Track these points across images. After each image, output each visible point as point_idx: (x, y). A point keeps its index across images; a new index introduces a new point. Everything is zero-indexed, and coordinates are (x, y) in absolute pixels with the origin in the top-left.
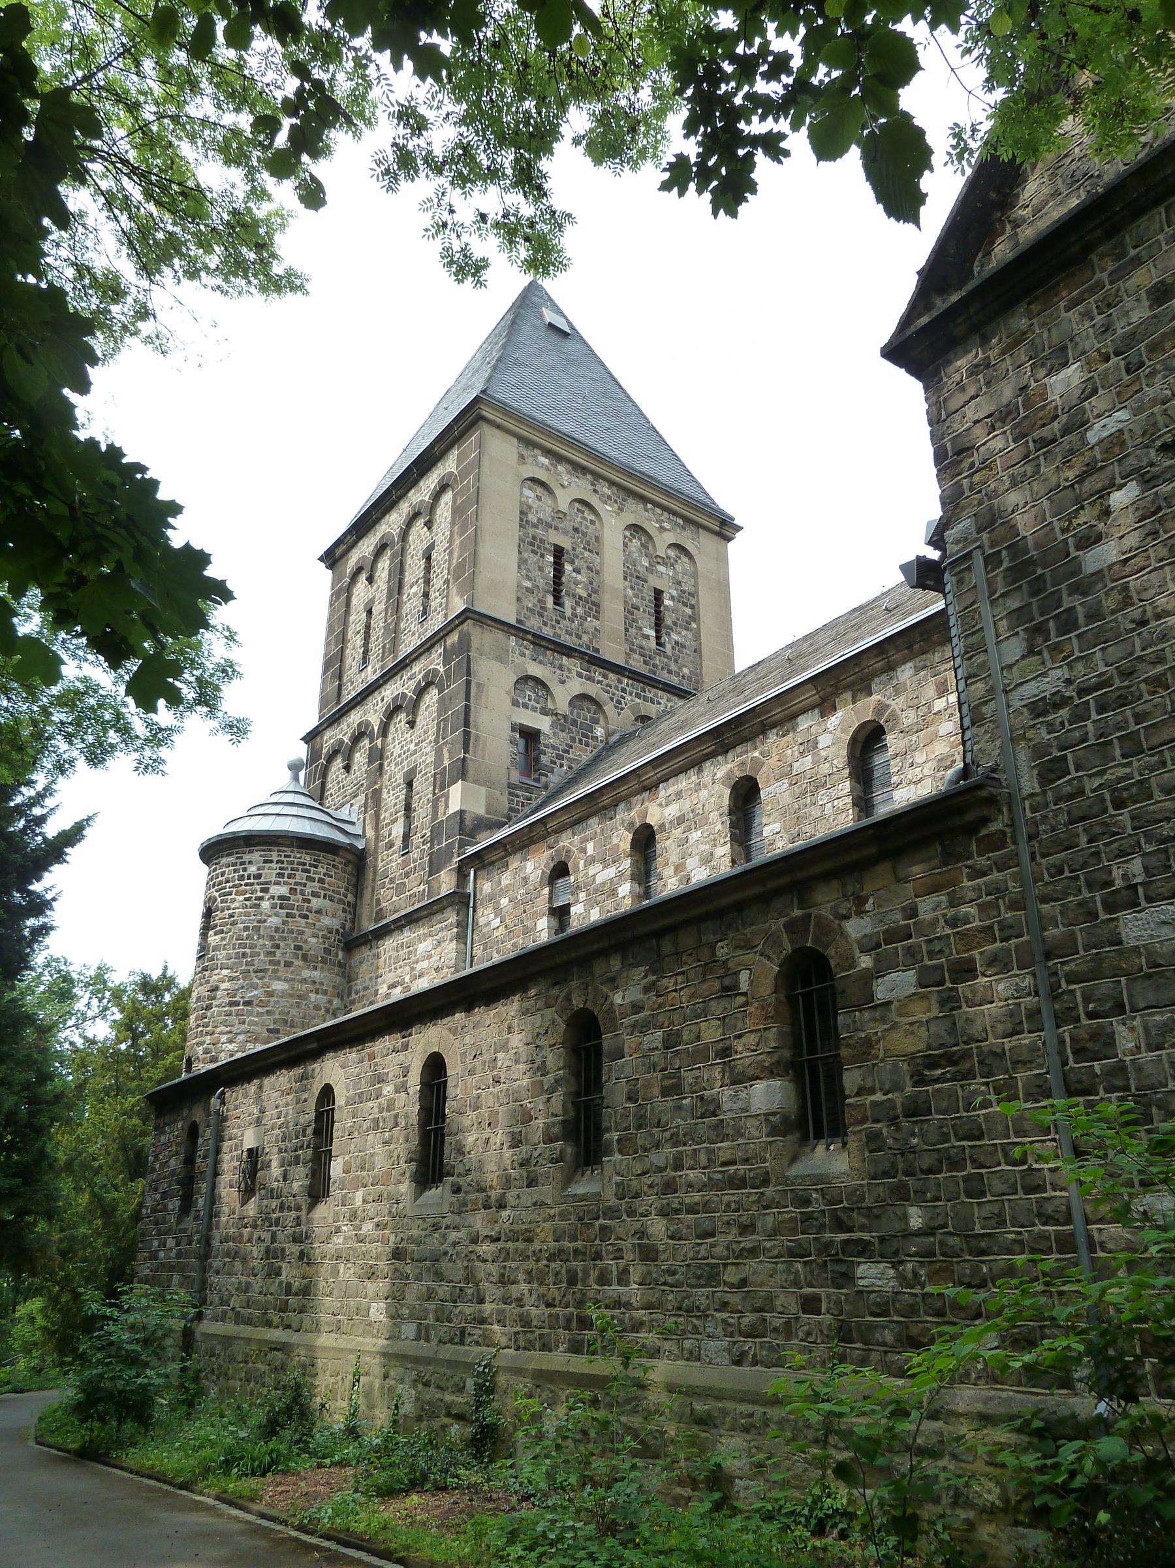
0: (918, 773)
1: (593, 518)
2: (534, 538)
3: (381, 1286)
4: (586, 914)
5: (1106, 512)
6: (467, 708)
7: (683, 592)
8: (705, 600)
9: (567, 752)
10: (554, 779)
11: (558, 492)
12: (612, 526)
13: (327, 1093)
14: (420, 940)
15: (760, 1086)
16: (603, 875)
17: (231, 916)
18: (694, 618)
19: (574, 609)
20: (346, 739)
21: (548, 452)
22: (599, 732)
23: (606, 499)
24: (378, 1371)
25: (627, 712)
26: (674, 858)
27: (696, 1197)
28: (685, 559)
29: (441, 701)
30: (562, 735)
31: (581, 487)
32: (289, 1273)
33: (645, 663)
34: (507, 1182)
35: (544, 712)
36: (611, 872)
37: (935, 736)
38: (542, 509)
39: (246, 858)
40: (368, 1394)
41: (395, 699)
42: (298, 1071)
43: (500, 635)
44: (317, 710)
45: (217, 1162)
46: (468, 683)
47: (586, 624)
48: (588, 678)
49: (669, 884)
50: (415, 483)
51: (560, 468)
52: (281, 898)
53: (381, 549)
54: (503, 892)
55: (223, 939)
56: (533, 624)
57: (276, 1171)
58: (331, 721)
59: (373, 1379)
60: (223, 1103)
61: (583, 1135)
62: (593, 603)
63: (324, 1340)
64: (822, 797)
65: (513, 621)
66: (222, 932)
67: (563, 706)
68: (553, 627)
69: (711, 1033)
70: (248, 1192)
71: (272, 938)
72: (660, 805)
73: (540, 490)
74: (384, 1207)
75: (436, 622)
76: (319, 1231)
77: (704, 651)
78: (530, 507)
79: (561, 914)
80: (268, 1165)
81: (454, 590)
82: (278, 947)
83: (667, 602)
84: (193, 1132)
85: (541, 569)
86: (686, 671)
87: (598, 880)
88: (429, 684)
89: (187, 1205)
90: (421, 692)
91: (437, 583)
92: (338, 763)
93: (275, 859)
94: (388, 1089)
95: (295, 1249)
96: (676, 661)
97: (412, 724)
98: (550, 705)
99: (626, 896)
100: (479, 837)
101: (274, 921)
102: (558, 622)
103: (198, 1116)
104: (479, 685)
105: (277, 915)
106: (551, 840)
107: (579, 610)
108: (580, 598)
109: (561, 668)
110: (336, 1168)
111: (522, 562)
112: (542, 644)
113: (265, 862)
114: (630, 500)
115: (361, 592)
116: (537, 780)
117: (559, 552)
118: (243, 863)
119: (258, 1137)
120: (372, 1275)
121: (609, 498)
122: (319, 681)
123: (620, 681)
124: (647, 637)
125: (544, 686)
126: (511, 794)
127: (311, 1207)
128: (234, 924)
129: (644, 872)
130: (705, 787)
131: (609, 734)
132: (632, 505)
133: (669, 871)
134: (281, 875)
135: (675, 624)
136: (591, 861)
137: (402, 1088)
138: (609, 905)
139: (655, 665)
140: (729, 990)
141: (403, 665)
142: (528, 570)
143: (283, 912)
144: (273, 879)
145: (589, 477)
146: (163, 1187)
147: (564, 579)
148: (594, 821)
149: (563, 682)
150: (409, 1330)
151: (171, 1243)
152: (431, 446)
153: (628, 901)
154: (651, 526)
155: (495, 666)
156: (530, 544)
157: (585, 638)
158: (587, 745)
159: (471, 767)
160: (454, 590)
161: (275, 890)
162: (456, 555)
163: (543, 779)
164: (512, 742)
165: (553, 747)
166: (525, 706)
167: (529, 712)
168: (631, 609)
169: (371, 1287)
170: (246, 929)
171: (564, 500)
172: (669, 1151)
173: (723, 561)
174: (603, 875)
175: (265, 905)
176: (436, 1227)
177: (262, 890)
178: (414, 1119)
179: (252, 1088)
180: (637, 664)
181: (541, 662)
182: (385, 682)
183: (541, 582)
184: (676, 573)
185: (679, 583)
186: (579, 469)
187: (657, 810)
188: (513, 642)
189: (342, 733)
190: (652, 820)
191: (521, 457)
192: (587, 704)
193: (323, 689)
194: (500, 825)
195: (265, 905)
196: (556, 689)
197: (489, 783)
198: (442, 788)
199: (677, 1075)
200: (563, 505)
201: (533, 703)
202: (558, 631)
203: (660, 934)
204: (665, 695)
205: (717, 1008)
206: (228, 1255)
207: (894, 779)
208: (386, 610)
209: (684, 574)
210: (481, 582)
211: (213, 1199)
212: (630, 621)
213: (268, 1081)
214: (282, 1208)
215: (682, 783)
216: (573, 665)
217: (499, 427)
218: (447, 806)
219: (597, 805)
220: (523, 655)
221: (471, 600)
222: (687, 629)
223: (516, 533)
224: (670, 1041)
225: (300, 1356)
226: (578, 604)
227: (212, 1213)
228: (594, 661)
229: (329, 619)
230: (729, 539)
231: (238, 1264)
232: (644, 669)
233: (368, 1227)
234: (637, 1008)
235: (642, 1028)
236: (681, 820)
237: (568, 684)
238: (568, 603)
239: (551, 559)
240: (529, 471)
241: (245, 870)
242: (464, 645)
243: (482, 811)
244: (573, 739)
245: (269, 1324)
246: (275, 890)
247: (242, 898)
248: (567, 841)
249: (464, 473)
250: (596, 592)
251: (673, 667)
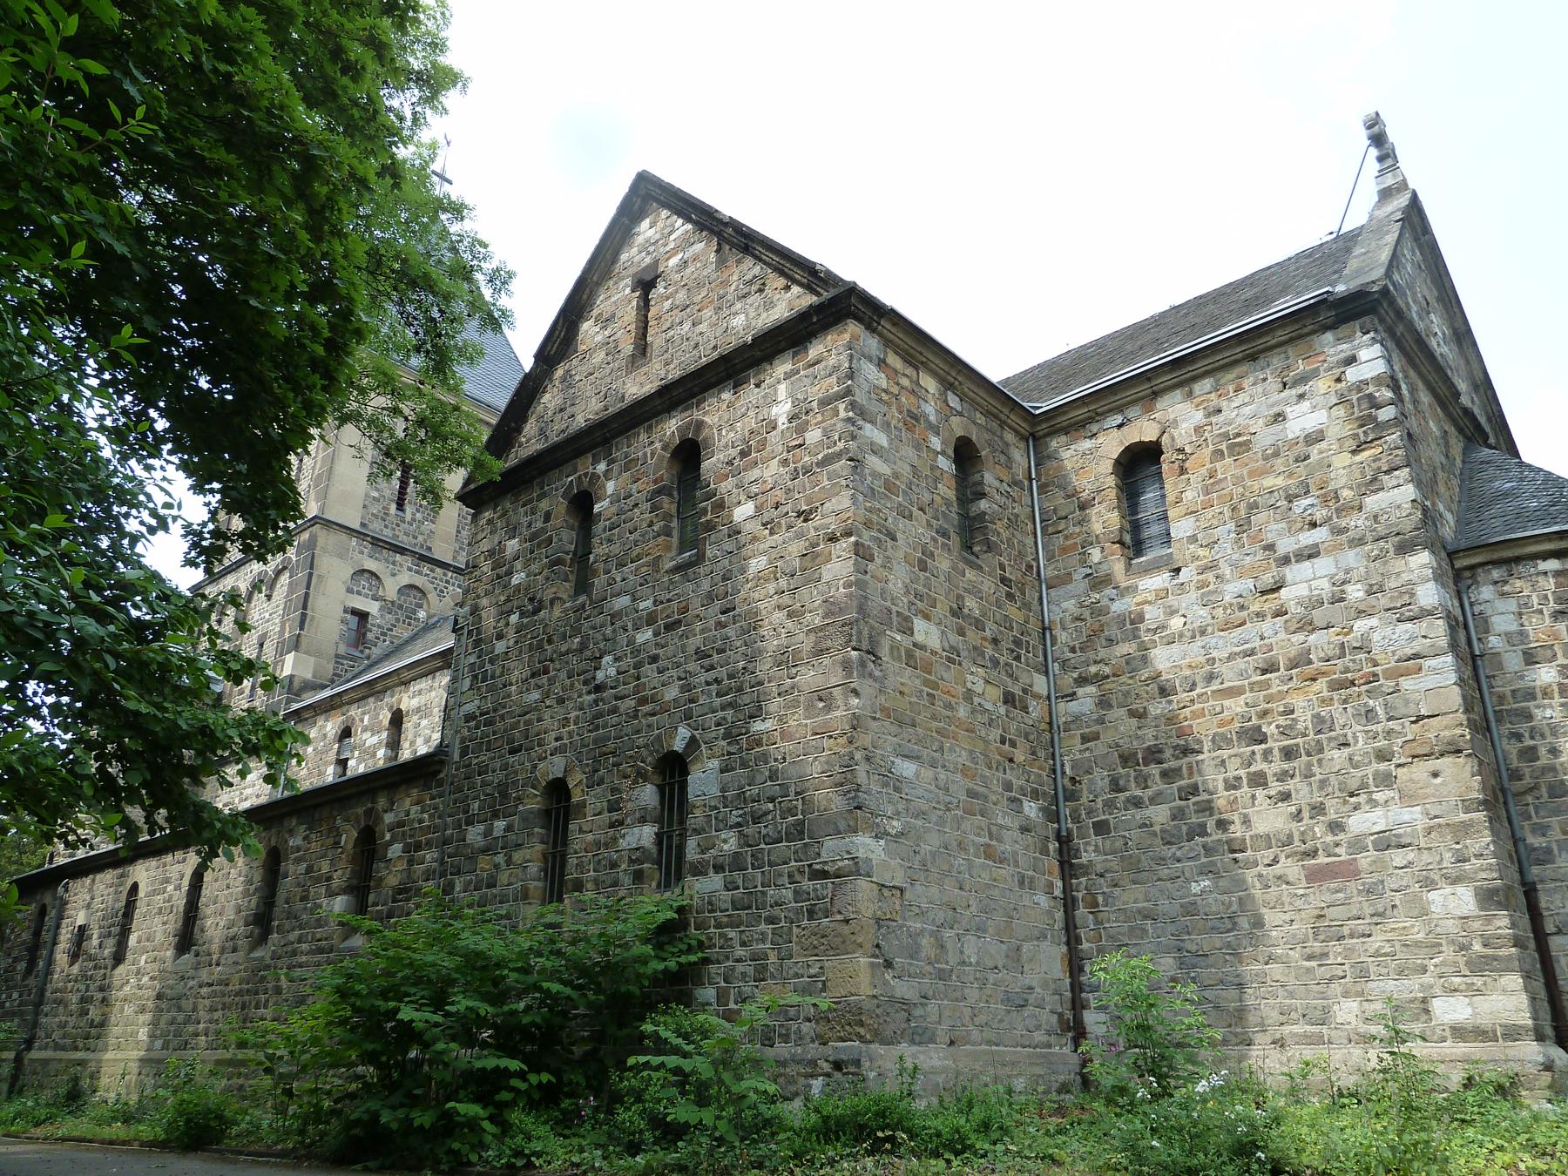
0: (421, 739)
3: (148, 1017)
4: (357, 767)
5: (508, 624)
6: (307, 595)
10: (376, 652)
13: (135, 888)
15: (339, 898)
16: (372, 740)
22: (422, 614)
24: (136, 1071)
27: (304, 958)
30: (388, 616)
32: (94, 1013)
34: (223, 950)
35: (375, 598)
36: (375, 740)
40: (127, 1087)
42: (120, 871)
43: (344, 537)
45: (56, 935)
46: (311, 575)
48: (417, 572)
49: (406, 755)
56: (376, 527)
57: (95, 942)
59: (132, 1078)
60: (67, 891)
61: (262, 921)
63: (109, 1055)
65: (356, 526)
69: (325, 868)
70: (74, 957)
74: (156, 966)
76: (116, 982)
79: (342, 763)
80: (90, 937)
84: (43, 912)
88: (285, 568)
89: (32, 963)
90: (278, 573)
94: (170, 888)
95: (100, 996)
97: (269, 597)
99: (381, 759)
103: (48, 899)
106: (344, 709)
107: (418, 516)
109: (394, 563)
110: (133, 940)
112: (377, 542)
119: (88, 917)
120: (143, 1010)
125: (378, 578)
127: (114, 968)
129: (394, 744)
131: (429, 617)
136: (365, 730)
137: (178, 888)
138: (370, 762)
140: (337, 844)
146: (15, 953)
148: (371, 700)
149: (394, 575)
150: (158, 1044)
151: (15, 995)
153: (381, 762)
155: (336, 561)
157: (420, 538)
159: (304, 641)
166: (359, 593)
169: (142, 1018)
172: (297, 933)
176: (183, 978)
178: (181, 909)
179: (88, 881)
187: (408, 700)
188: (354, 542)
190: (403, 707)
192: (415, 592)
194: (324, 687)
197: (317, 654)
199: (307, 891)
203: (316, 806)
205: (330, 853)
206: (55, 1001)
210: (334, 492)
211: (50, 961)
213: (99, 877)
214: (95, 968)
215: (423, 684)
216: (406, 561)
219: (373, 690)
224: (309, 870)
225: (92, 1067)
227: (49, 972)
231: (61, 1009)
233: (145, 979)
234: (298, 849)
235: (298, 861)
236: (418, 710)
237: (398, 576)
242: (312, 544)
243: (309, 676)
244: (398, 620)
245: (76, 1049)
248: (354, 711)
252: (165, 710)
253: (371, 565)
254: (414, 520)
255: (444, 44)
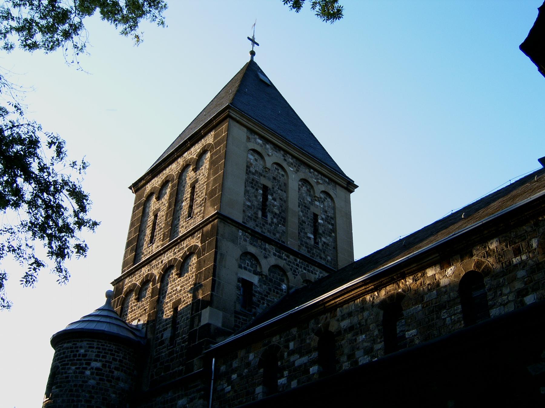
1: (283, 173)
2: (253, 180)
7: (328, 216)
8: (339, 221)
9: (267, 296)
10: (259, 311)
11: (266, 158)
12: (293, 180)
14: (179, 398)
17: (67, 377)
18: (334, 230)
19: (272, 219)
20: (138, 283)
21: (262, 137)
23: (290, 164)
25: (299, 277)
26: (346, 351)
28: (329, 200)
29: (199, 262)
30: (264, 286)
31: (278, 157)
33: (309, 252)
35: (255, 273)
36: (305, 359)
37: (515, 279)
38: (258, 166)
39: (79, 344)
41: (170, 262)
43: (234, 229)
44: (121, 268)
47: (278, 228)
48: (280, 257)
50: (188, 149)
51: (268, 146)
52: (97, 369)
53: (165, 184)
54: (234, 371)
55: (61, 391)
56: (251, 224)
58: (130, 274)
62: (282, 217)
64: (444, 314)
66: (60, 386)
67: (265, 270)
68: (261, 228)
71: (90, 392)
72: (338, 320)
73: (257, 156)
75: (198, 220)
77: (339, 248)
78: (251, 164)
81: (208, 204)
82: (93, 397)
83: (320, 221)
85: (256, 197)
86: (329, 258)
87: (297, 363)
90: (187, 258)
91: (198, 200)
92: (133, 297)
93: (95, 346)
96: (324, 252)
98: (258, 270)
100: (218, 340)
101: (92, 382)
102: (263, 225)
104: (221, 254)
105: (94, 379)
108: (276, 214)
109: (265, 249)
111: (246, 192)
112: (257, 237)
113: (90, 347)
114: (302, 166)
115: (154, 204)
116: (250, 311)
117: (265, 189)
118: (77, 347)
121: (292, 164)
122: (124, 252)
123: (296, 260)
124: (309, 238)
126: (235, 317)
128: (69, 382)
130: (367, 310)
131: (289, 288)
132: (303, 169)
133: (344, 358)
134: (98, 356)
135: (324, 233)
139: (313, 254)
141: (176, 243)
142: (249, 196)
143: (98, 377)
144: (93, 358)
145: (282, 152)
147: (268, 203)
149: (266, 257)
152: (200, 130)
154: (313, 181)
156: (251, 183)
157: (278, 235)
158: (277, 293)
160: (208, 204)
161: (94, 364)
162: (211, 185)
163: (254, 310)
164: (238, 288)
165: (259, 293)
166: (245, 269)
167: (247, 272)
168: (301, 223)
170: (75, 386)
171: (269, 162)
173: (348, 203)
174: (299, 361)
175: (88, 373)
177: (87, 364)
180: (303, 251)
181: (254, 245)
182: (164, 253)
183: (256, 203)
184: (324, 206)
185: (326, 212)
186: (277, 148)
188: (240, 233)
189: (136, 280)
191: (248, 139)
193: (125, 257)
194: (229, 334)
195: (88, 373)
196: (263, 262)
198: (197, 311)
200: (269, 164)
201: (249, 267)
202: (264, 230)
204: (319, 270)
207: (490, 303)
208: (167, 214)
209: (329, 207)
212: (301, 229)
217: (238, 122)
218: (200, 321)
220: (245, 240)
221: (220, 208)
222: (330, 236)
223: (244, 176)
226: (274, 217)
228: (282, 248)
229: (131, 220)
230: (352, 192)
232: (308, 255)
236: (351, 328)
238: (269, 216)
239: (261, 192)
240: (251, 146)
241: (77, 351)
243: (220, 325)
244: (270, 289)
246: (94, 364)
247: (74, 368)
249: (217, 144)
250: (283, 211)
251: (323, 256)
252: (183, 248)
253: (252, 249)
254: (272, 222)
255: (19, 206)
